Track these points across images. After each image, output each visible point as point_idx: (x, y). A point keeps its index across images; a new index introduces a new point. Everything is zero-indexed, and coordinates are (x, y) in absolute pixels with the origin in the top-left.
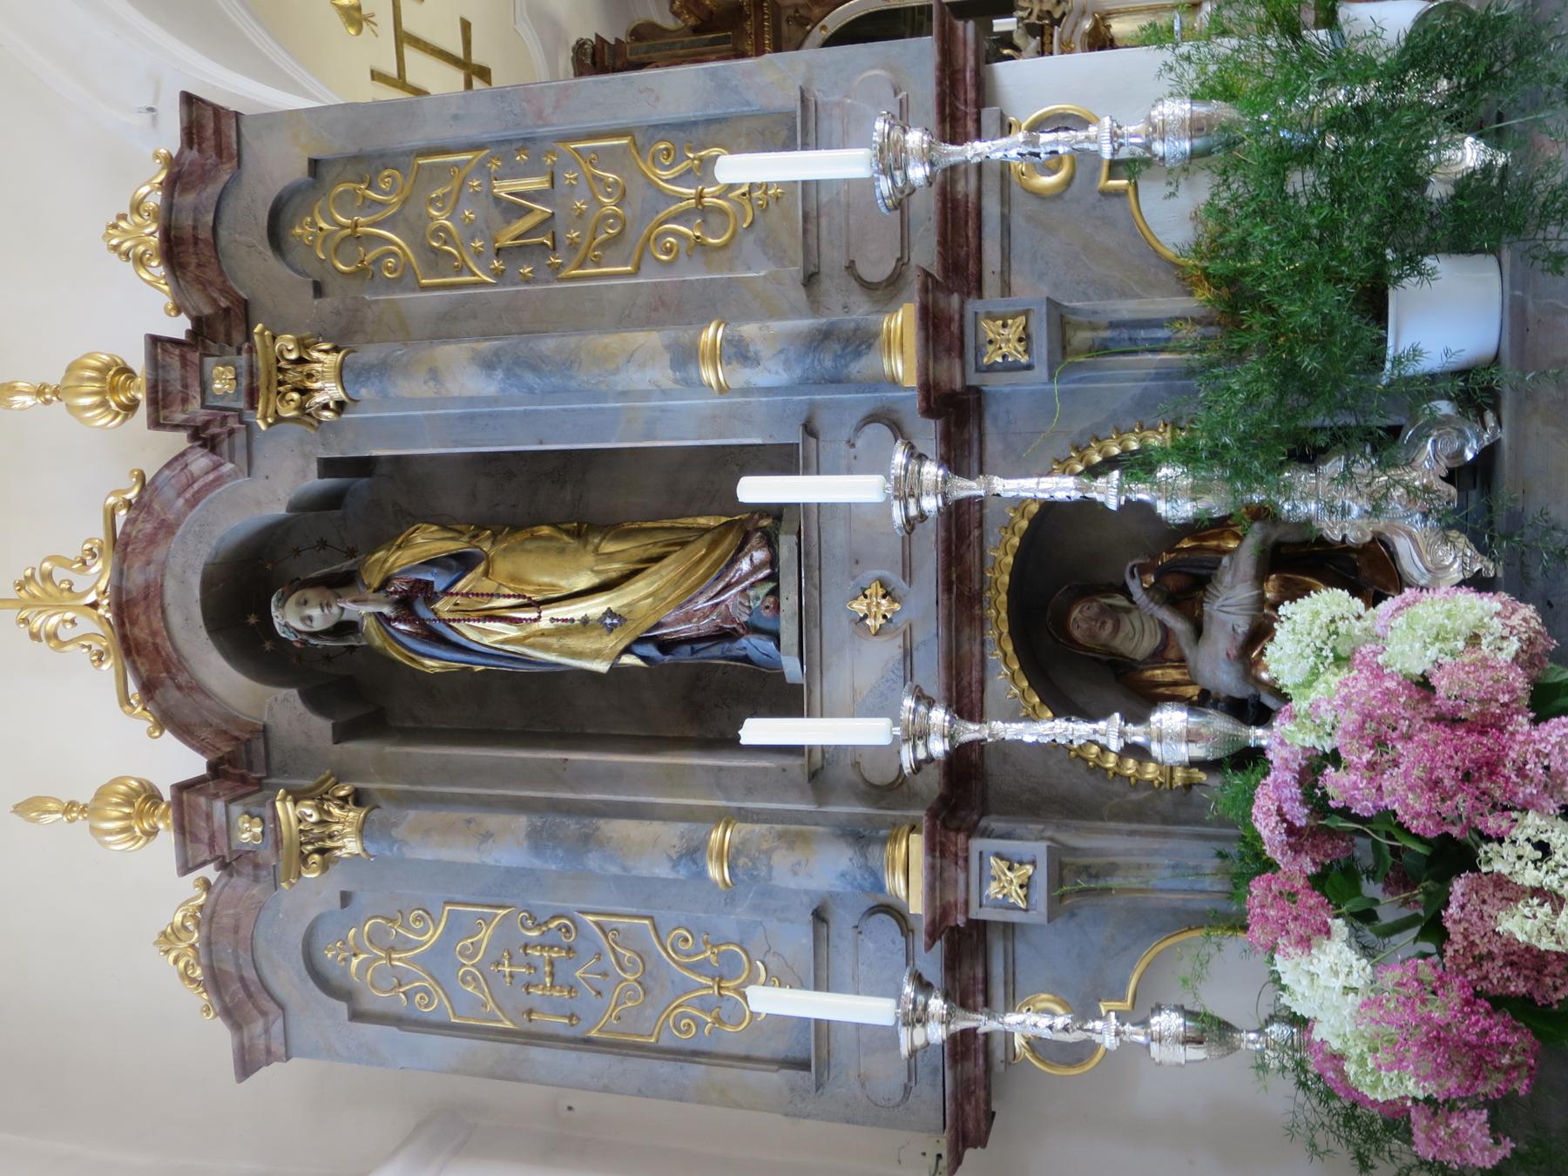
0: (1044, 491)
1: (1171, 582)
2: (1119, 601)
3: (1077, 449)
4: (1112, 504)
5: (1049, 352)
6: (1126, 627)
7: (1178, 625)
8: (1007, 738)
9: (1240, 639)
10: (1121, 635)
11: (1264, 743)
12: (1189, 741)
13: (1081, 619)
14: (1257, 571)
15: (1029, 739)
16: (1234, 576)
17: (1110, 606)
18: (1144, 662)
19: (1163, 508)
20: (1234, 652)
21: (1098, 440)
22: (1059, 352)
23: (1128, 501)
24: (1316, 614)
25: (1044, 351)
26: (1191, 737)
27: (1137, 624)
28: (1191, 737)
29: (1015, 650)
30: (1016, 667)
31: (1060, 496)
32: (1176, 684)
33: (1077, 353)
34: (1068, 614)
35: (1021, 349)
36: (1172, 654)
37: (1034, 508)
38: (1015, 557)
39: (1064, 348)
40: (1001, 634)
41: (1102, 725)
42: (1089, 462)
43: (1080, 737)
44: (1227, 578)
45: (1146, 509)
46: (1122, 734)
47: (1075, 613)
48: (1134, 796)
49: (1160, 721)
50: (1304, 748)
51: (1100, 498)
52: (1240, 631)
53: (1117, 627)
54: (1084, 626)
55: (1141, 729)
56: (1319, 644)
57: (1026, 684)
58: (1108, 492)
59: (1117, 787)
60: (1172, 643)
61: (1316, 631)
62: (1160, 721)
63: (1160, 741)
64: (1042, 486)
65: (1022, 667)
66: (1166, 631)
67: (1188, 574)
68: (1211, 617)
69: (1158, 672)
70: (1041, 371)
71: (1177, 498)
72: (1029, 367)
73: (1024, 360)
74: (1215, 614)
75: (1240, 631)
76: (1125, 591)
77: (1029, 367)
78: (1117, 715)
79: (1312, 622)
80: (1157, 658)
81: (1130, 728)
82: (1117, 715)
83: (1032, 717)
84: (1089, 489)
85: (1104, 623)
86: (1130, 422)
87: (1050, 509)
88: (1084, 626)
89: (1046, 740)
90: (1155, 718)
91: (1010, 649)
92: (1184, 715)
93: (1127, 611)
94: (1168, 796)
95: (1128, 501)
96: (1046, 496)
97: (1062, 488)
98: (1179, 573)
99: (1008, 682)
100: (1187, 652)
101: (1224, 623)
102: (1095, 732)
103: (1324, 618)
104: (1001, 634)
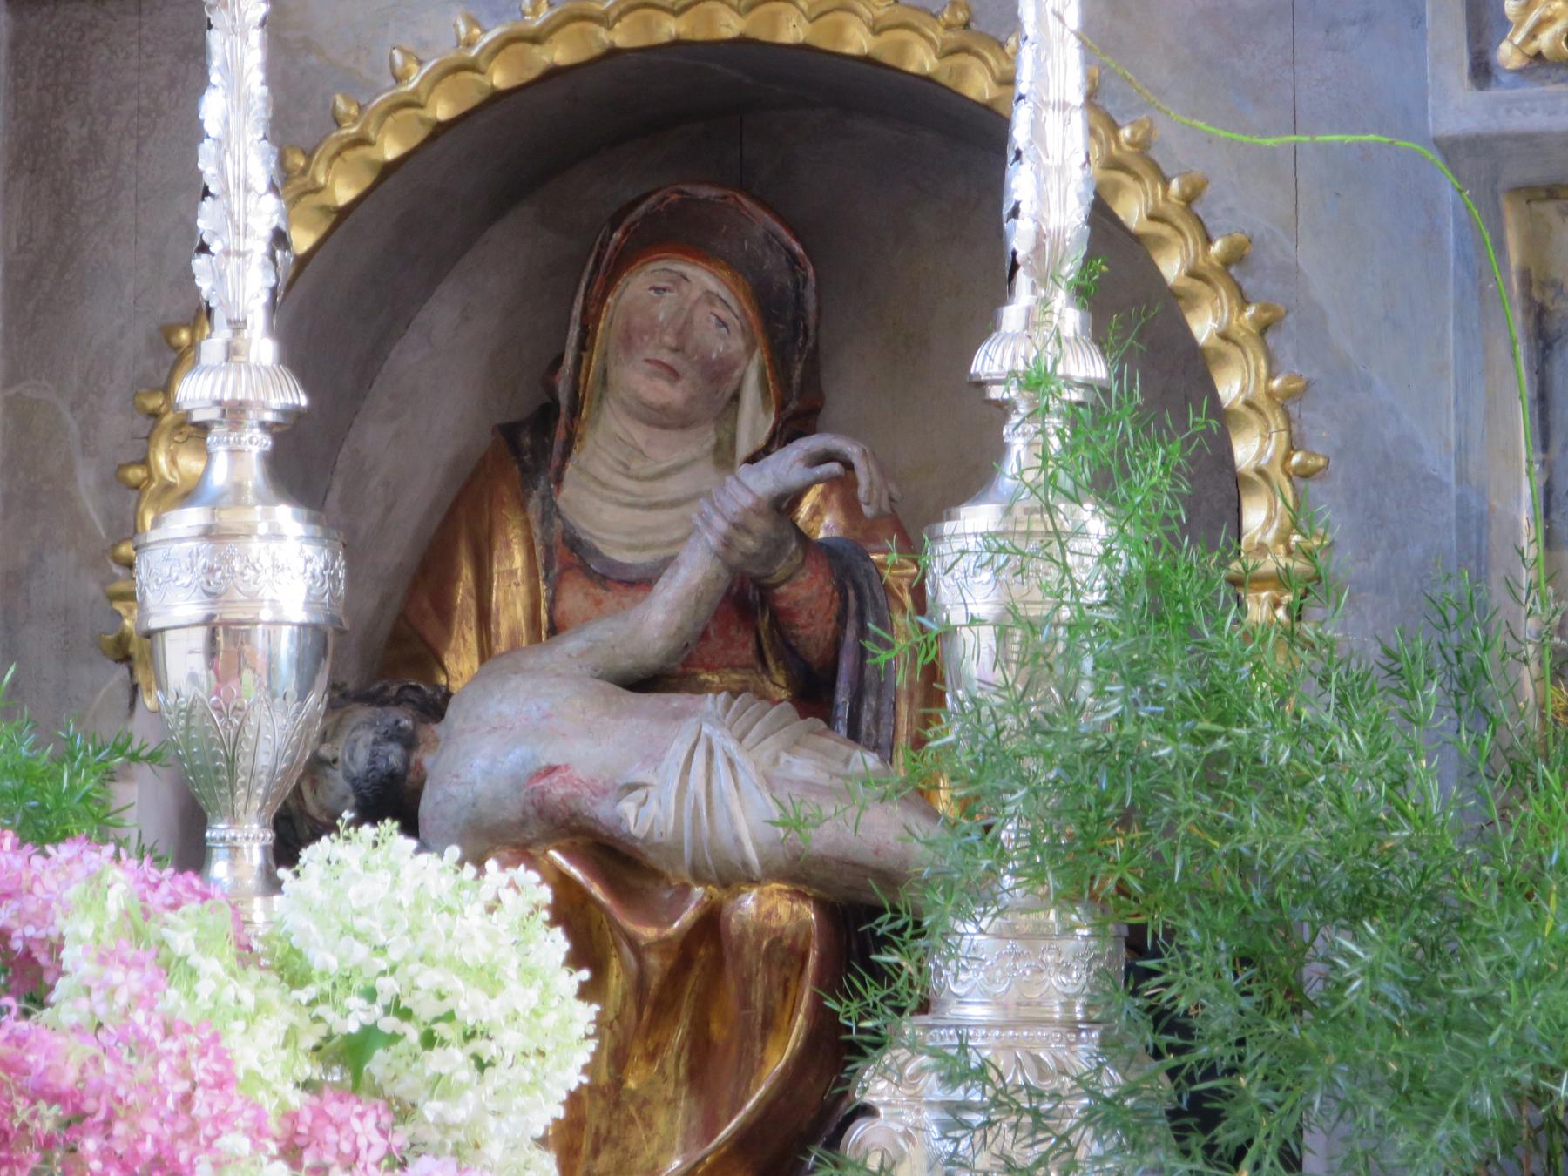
0: (1036, 126)
1: (806, 593)
2: (754, 422)
3: (1235, 258)
4: (990, 361)
5: (1530, 140)
6: (665, 449)
7: (655, 622)
8: (215, 39)
9: (603, 811)
10: (639, 434)
11: (219, 868)
12: (212, 626)
13: (682, 304)
14: (822, 861)
15: (213, 108)
16: (808, 786)
17: (736, 397)
18: (550, 512)
19: (975, 520)
20: (557, 790)
21: (1264, 329)
22: (1534, 173)
23: (1004, 409)
24: (488, 979)
25: (1538, 121)
26: (224, 638)
27: (675, 487)
28: (224, 638)
29: (554, 74)
30: (499, 78)
31: (1021, 183)
32: (484, 617)
33: (1536, 241)
34: (699, 251)
35: (1545, 41)
36: (574, 598)
37: (979, 86)
38: (867, 60)
39: (1551, 192)
40: (603, 20)
41: (263, 349)
42: (1192, 301)
43: (220, 277)
44: (803, 767)
45: (972, 474)
46: (234, 413)
47: (703, 278)
48: (86, 478)
49: (276, 535)
50: (56, 948)
51: (1012, 316)
52: (628, 807)
53: (663, 419)
54: (663, 310)
55: (253, 473)
56: (388, 987)
57: (442, 111)
58: (1038, 341)
59: (115, 424)
60: (610, 599)
61: (428, 979)
62: (276, 535)
63: (210, 533)
64: (1052, 120)
65: (497, 97)
66: (641, 582)
67: (836, 645)
68: (678, 716)
69: (519, 561)
70: (1459, 109)
71: (1006, 575)
72: (1482, 70)
73: (1508, 54)
74: (688, 730)
75: (628, 807)
76: (783, 435)
77: (1482, 70)
78: (303, 401)
79: (463, 970)
80: (569, 559)
81: (257, 443)
82: (303, 401)
83: (296, 128)
84: (1043, 279)
85: (673, 374)
86: (1324, 435)
87: (973, 141)
88: (663, 310)
89: (207, 166)
90: (287, 517)
91: (559, 53)
92: (298, 613)
93: (724, 456)
94: (93, 589)
95: (1004, 409)
96: (1020, 134)
97: (1048, 188)
98: (842, 619)
99: (448, 52)
100: (571, 644)
101: (653, 759)
102: (237, 326)
103: (471, 1005)
104: (603, 20)
